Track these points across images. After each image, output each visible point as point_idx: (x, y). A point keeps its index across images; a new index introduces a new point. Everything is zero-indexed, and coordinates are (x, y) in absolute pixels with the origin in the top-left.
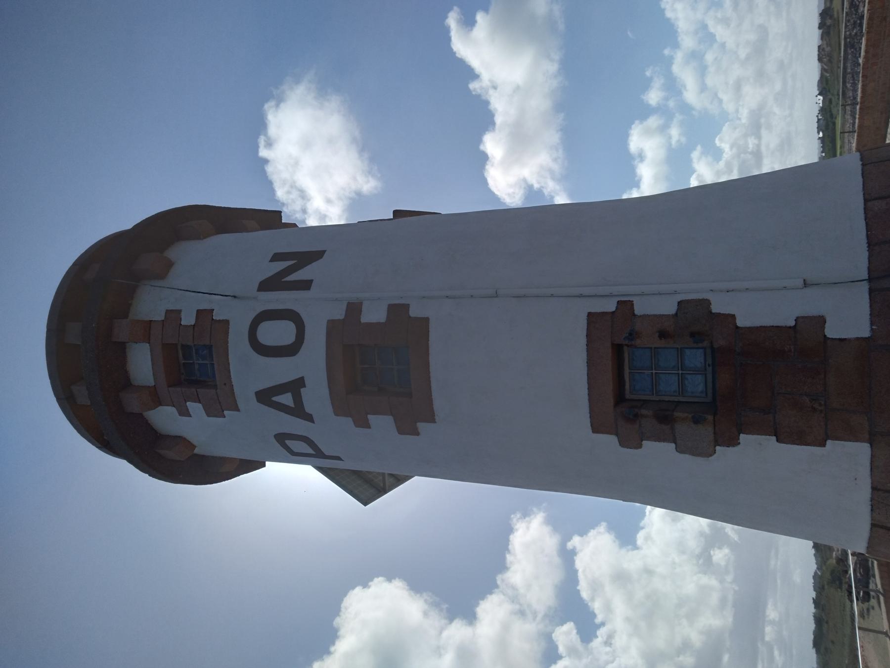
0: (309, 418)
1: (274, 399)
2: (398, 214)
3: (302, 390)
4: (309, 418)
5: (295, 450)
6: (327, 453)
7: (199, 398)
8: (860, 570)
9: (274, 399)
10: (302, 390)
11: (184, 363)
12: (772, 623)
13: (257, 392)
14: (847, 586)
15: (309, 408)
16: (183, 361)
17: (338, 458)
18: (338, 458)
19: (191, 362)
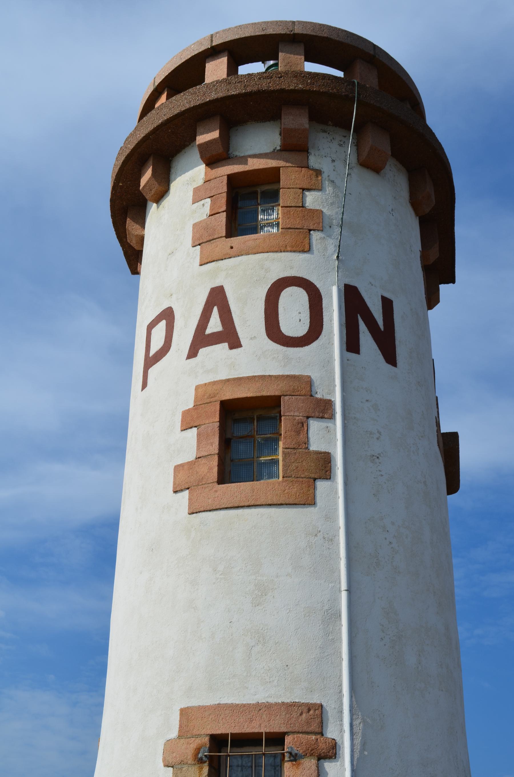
0: (193, 353)
1: (215, 309)
2: (433, 360)
3: (226, 345)
4: (193, 353)
5: (154, 331)
6: (150, 371)
7: (215, 214)
8: (275, 225)
9: (215, 309)
10: (226, 345)
11: (257, 191)
12: (232, 70)
13: (223, 288)
14: (196, 408)
15: (203, 351)
16: (259, 191)
17: (144, 385)
18: (144, 385)
19: (259, 202)
